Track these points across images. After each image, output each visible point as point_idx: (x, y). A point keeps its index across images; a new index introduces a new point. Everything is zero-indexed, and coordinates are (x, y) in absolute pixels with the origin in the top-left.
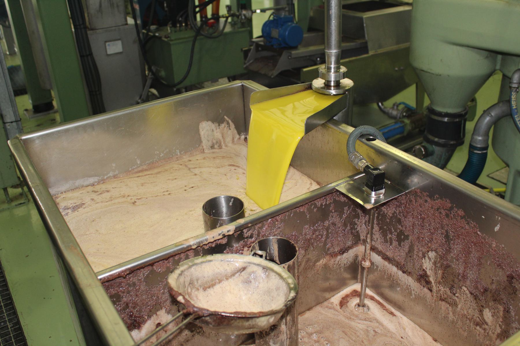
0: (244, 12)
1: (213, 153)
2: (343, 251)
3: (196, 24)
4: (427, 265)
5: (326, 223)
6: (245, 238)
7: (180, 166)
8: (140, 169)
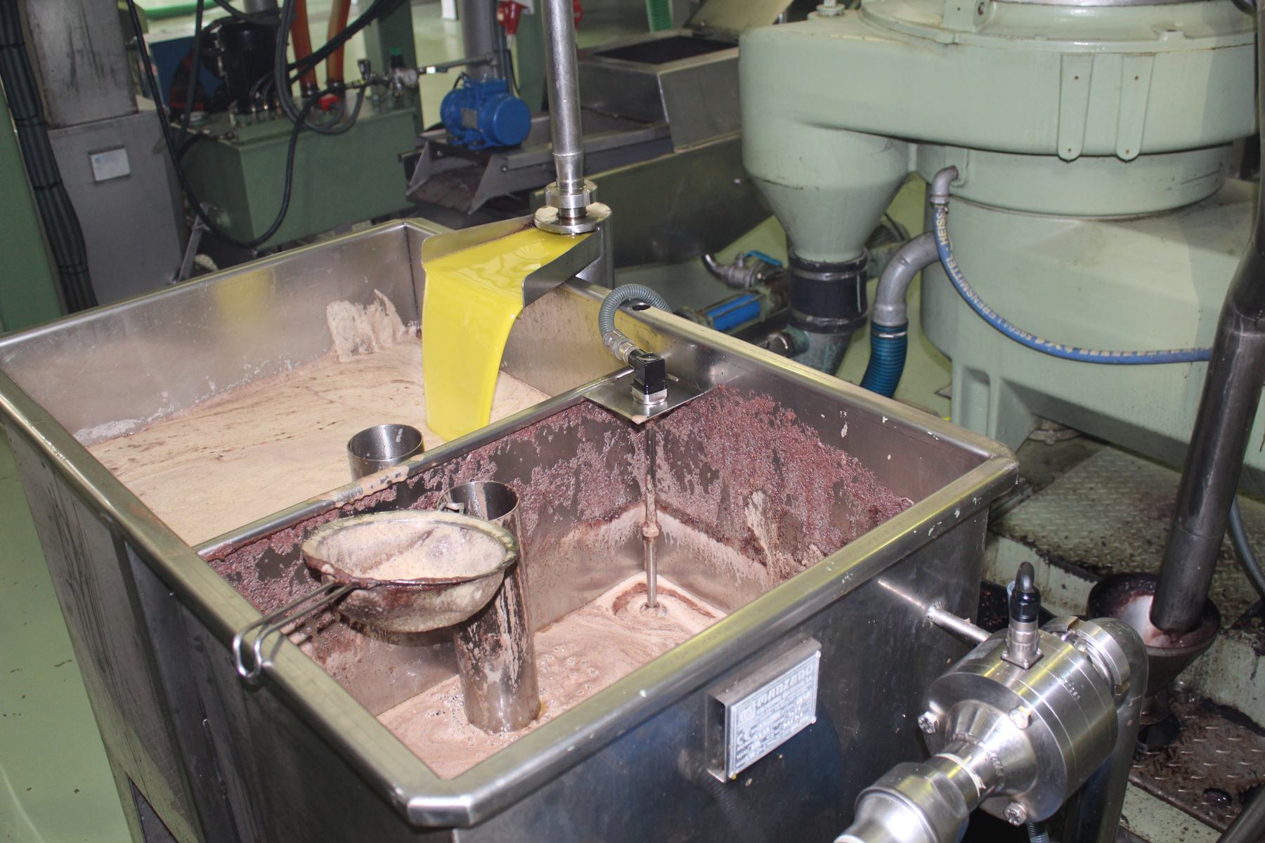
0: (399, 74)
1: (358, 361)
2: (610, 516)
3: (295, 106)
4: (753, 518)
5: (573, 463)
6: (426, 491)
7: (297, 390)
8: (217, 400)
